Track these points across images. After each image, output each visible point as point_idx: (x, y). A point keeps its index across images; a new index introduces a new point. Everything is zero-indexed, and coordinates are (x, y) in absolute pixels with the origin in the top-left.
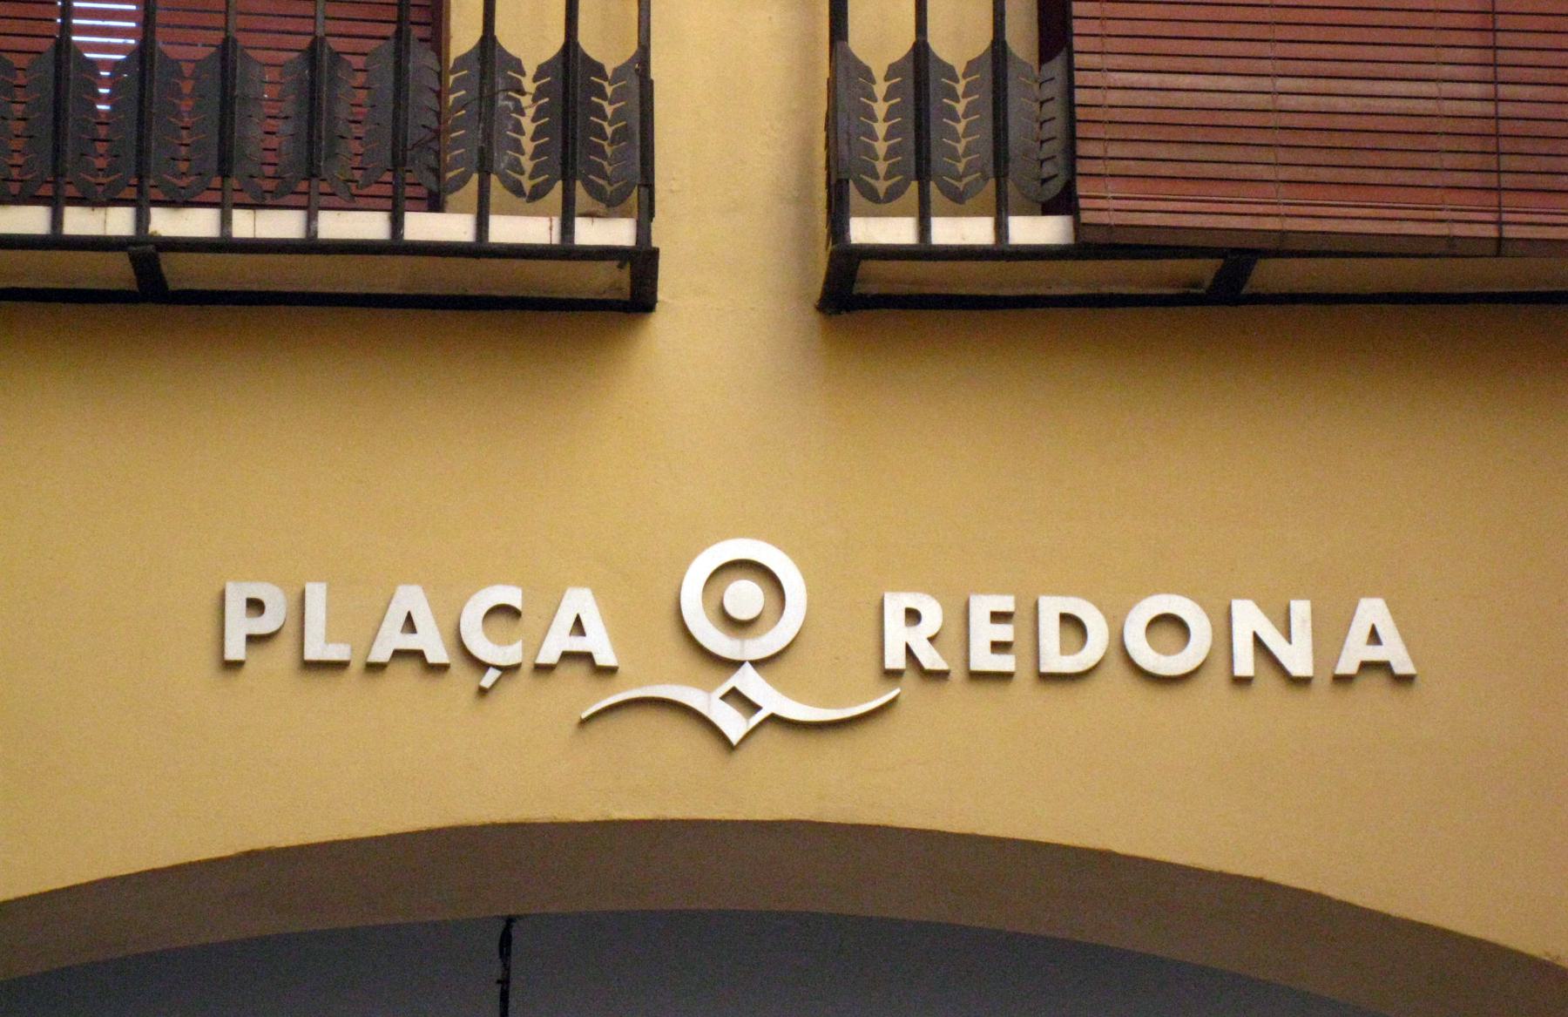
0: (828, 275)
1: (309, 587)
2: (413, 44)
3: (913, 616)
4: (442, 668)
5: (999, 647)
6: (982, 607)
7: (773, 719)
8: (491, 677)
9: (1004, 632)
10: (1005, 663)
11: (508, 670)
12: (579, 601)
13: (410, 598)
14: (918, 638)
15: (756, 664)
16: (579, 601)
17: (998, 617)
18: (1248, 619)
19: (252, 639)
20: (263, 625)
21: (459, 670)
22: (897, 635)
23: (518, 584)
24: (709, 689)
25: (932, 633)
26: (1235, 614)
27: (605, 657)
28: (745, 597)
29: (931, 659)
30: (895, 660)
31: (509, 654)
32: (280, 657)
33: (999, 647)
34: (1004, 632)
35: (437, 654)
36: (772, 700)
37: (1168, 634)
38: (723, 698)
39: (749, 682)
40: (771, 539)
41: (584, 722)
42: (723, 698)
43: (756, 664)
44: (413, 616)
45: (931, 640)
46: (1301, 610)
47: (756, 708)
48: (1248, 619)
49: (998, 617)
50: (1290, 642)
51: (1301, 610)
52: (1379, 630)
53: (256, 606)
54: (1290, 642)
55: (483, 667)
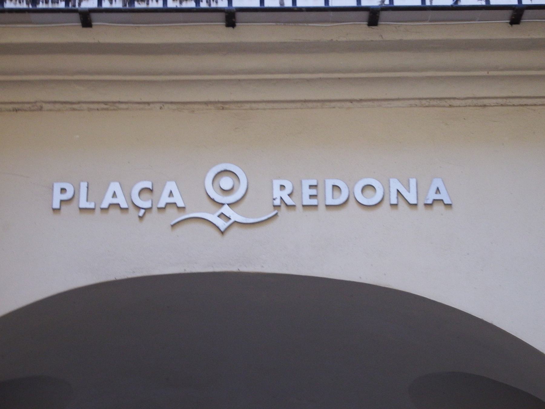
0: (131, 44)
1: (411, 180)
2: (132, 7)
3: (282, 187)
4: (127, 209)
5: (311, 196)
6: (306, 183)
7: (235, 222)
8: (142, 211)
9: (313, 192)
10: (314, 202)
11: (147, 210)
12: (171, 186)
13: (115, 187)
14: (284, 195)
15: (228, 204)
16: (171, 186)
17: (311, 187)
18: (395, 185)
19: (62, 201)
20: (288, 190)
21: (132, 210)
22: (277, 193)
23: (149, 180)
24: (213, 213)
25: (289, 192)
26: (303, 183)
27: (180, 204)
28: (226, 182)
29: (289, 201)
30: (277, 202)
31: (147, 205)
32: (73, 207)
33: (311, 196)
34: (313, 192)
35: (124, 205)
36: (235, 217)
37: (368, 192)
38: (219, 216)
39: (226, 210)
40: (225, 162)
41: (173, 226)
42: (219, 216)
43: (228, 204)
44: (114, 192)
45: (289, 195)
46: (413, 182)
47: (229, 219)
48: (395, 185)
49: (311, 187)
50: (409, 192)
51: (413, 182)
52: (440, 189)
53: (63, 190)
54: (409, 192)
55: (139, 208)
